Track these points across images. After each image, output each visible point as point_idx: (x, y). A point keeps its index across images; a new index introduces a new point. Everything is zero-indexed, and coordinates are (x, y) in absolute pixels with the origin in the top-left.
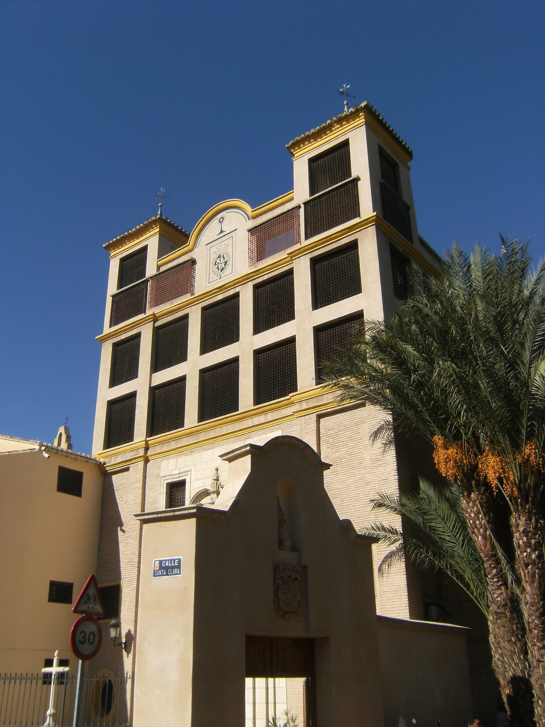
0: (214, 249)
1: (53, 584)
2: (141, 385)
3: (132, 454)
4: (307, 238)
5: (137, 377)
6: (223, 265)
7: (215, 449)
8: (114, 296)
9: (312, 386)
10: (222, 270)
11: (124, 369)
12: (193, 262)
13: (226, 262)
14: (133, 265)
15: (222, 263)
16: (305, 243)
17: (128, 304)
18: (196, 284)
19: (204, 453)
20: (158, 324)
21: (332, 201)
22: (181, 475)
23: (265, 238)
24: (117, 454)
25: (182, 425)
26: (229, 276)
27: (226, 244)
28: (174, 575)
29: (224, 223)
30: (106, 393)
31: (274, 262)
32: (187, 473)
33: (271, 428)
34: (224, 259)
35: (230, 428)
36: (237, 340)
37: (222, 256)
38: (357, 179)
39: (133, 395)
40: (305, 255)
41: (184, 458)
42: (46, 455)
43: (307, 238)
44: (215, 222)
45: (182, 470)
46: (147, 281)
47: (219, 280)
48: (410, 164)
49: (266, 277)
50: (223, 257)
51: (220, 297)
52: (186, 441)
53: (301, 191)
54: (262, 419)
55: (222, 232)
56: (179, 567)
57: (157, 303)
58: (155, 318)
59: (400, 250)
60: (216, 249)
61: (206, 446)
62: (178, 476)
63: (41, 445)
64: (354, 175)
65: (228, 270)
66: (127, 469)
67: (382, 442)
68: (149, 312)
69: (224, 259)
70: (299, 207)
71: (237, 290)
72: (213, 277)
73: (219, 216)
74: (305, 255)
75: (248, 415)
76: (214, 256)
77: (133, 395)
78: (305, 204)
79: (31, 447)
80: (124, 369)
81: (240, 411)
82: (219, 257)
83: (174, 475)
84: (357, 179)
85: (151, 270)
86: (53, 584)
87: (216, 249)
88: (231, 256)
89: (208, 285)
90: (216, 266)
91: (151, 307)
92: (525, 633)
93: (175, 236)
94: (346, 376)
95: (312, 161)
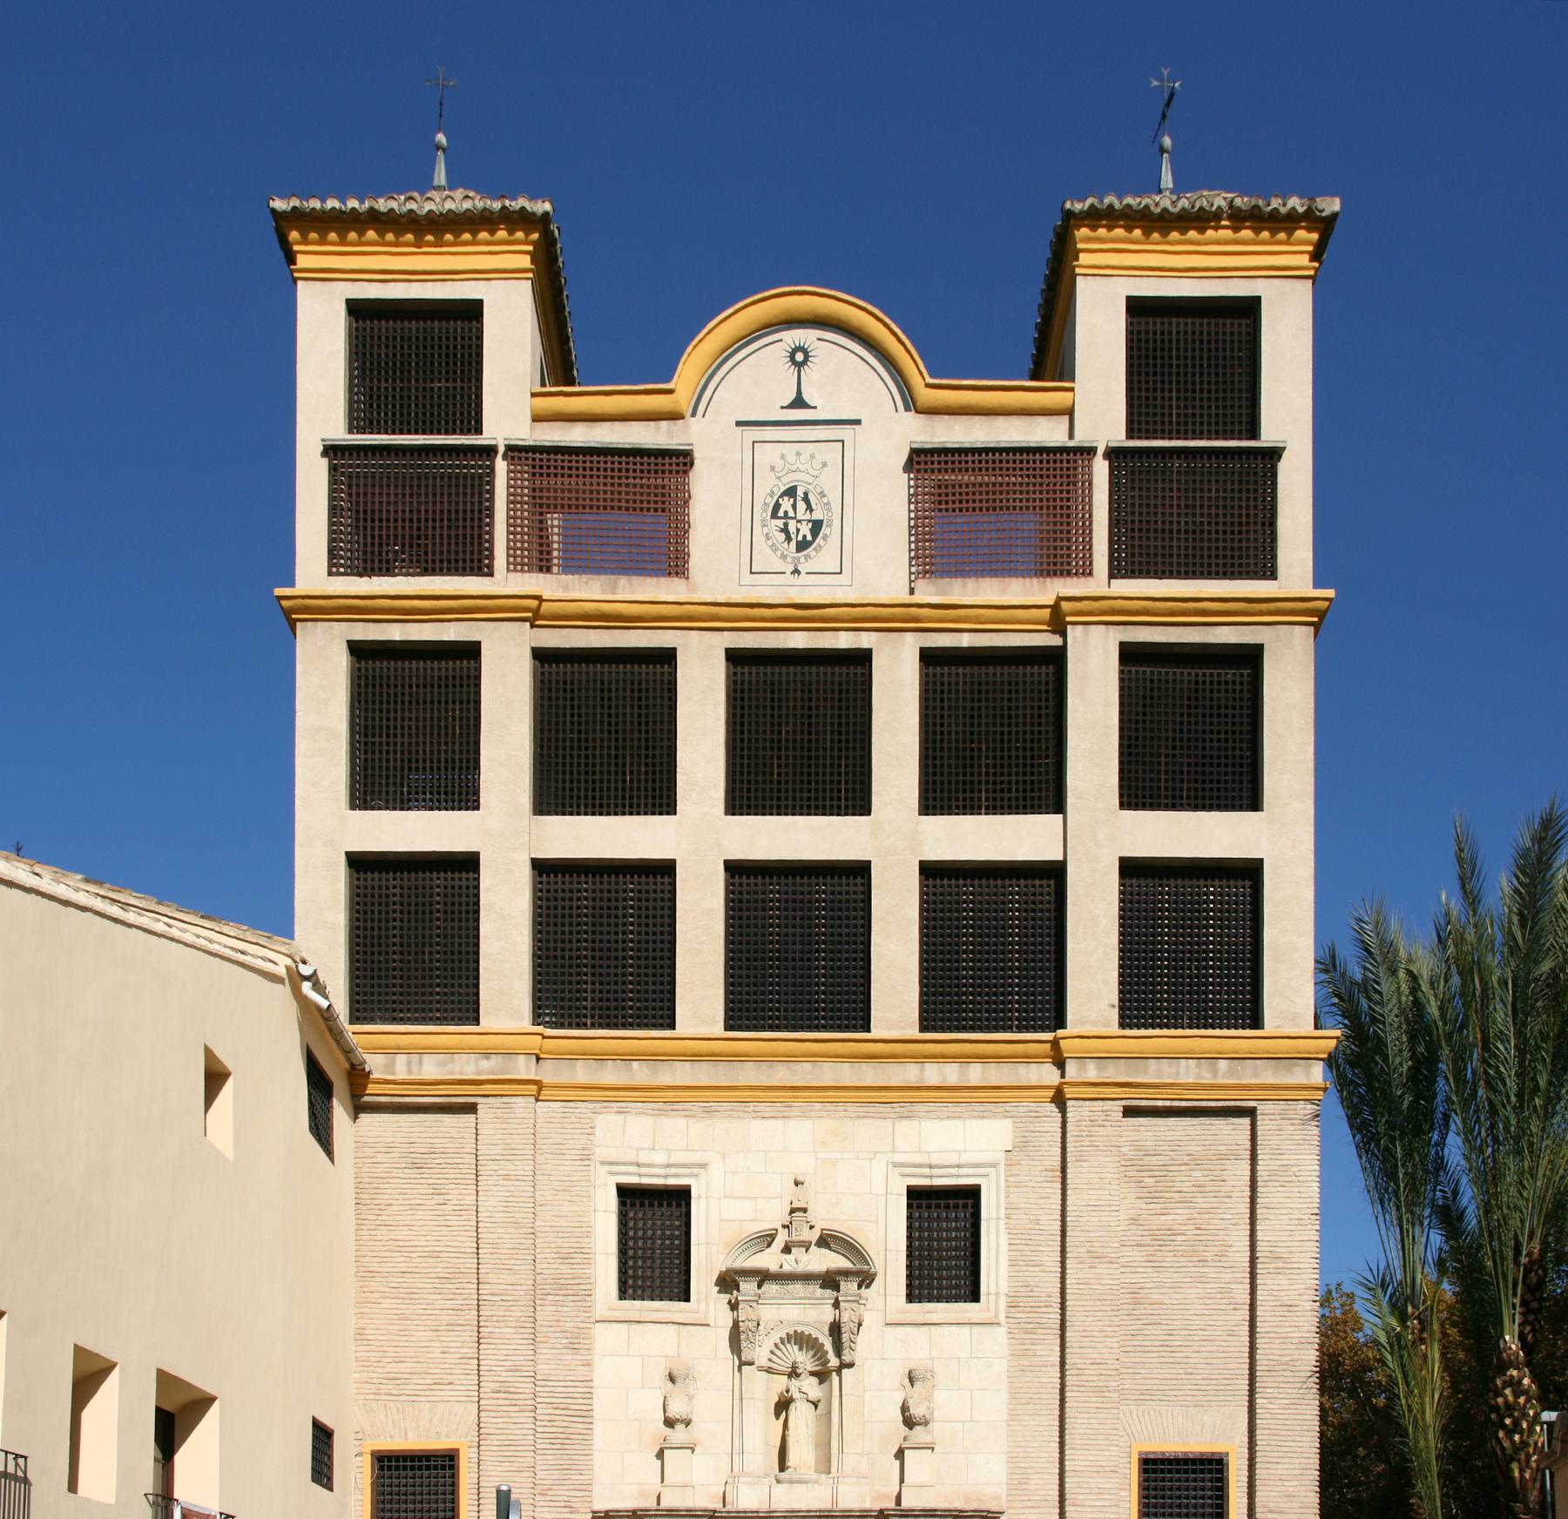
3: (485, 1064)
6: (805, 530)
7: (792, 1124)
9: (1108, 1025)
10: (803, 546)
13: (817, 526)
14: (414, 357)
19: (757, 1124)
24: (422, 1051)
27: (820, 458)
31: (1001, 604)
32: (695, 1171)
33: (977, 1107)
34: (809, 508)
35: (831, 1073)
37: (800, 492)
38: (1274, 454)
45: (678, 1157)
47: (789, 578)
49: (966, 641)
50: (806, 499)
51: (798, 640)
52: (681, 1074)
54: (933, 1074)
55: (799, 402)
61: (761, 1107)
66: (471, 1109)
69: (809, 508)
71: (864, 640)
81: (876, 1033)
82: (791, 492)
83: (938, 1167)
84: (1274, 454)
89: (748, 579)
90: (780, 523)
94: (324, 212)
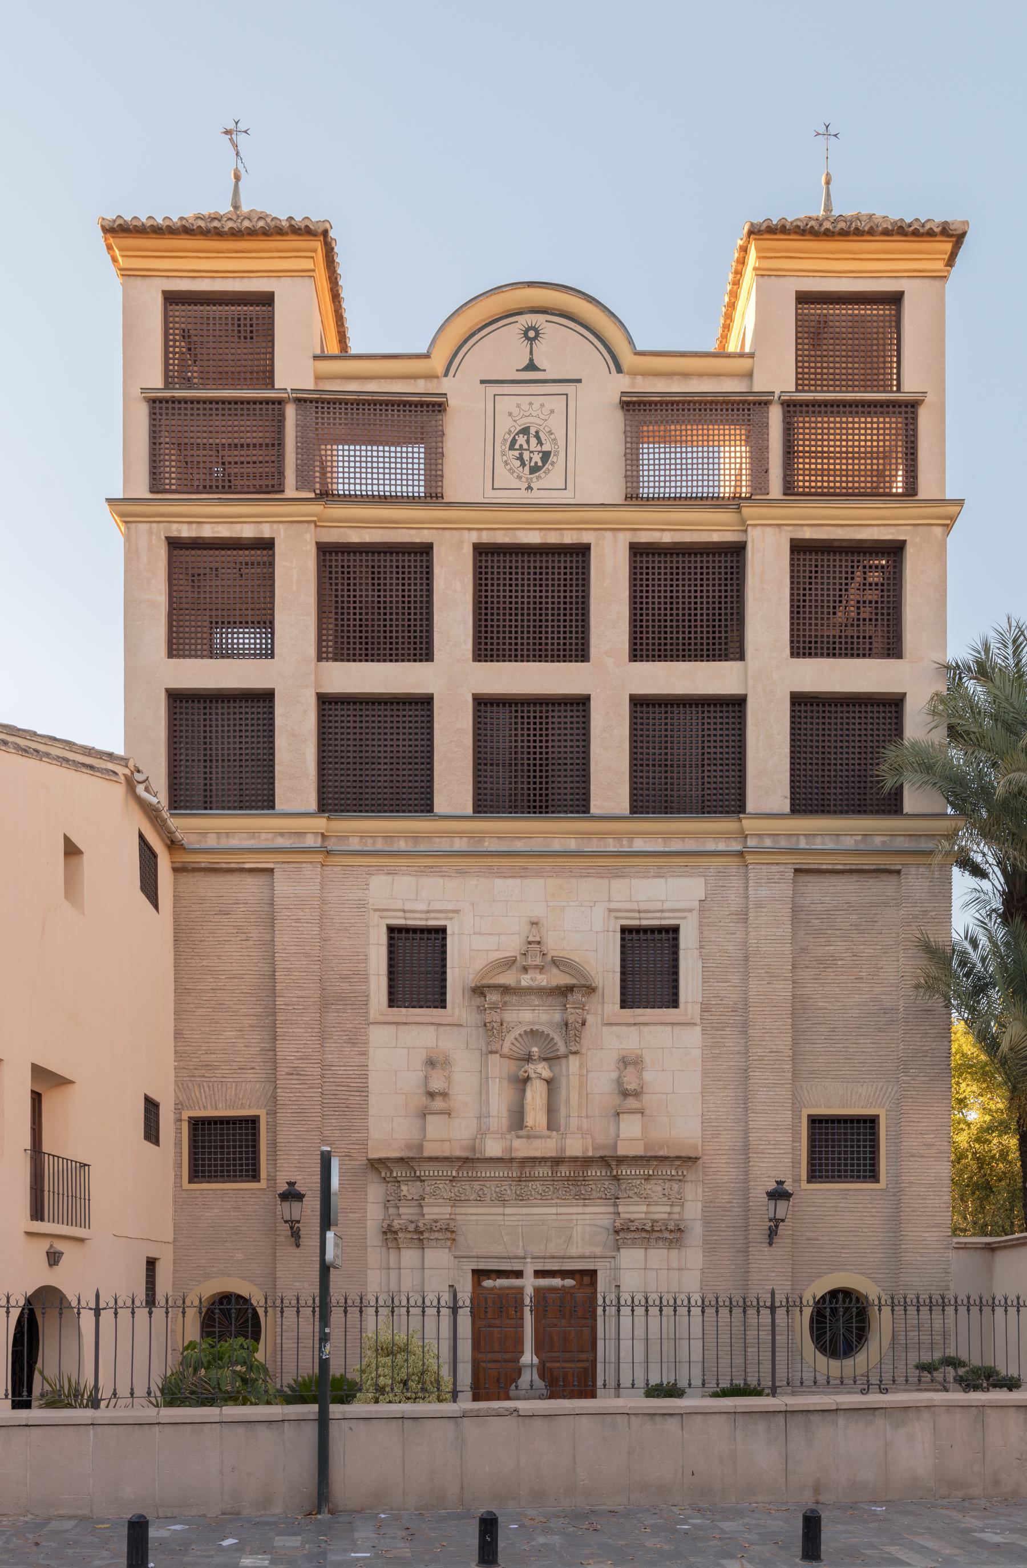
6: (537, 458)
7: (528, 882)
22: (432, 915)
32: (450, 915)
34: (540, 442)
37: (532, 431)
40: (541, 529)
41: (441, 880)
55: (531, 366)
62: (423, 916)
67: (977, 915)
69: (540, 442)
71: (585, 538)
74: (541, 529)
76: (506, 426)
81: (262, 1113)
82: (525, 431)
88: (562, 443)
90: (517, 453)
92: (1015, 641)
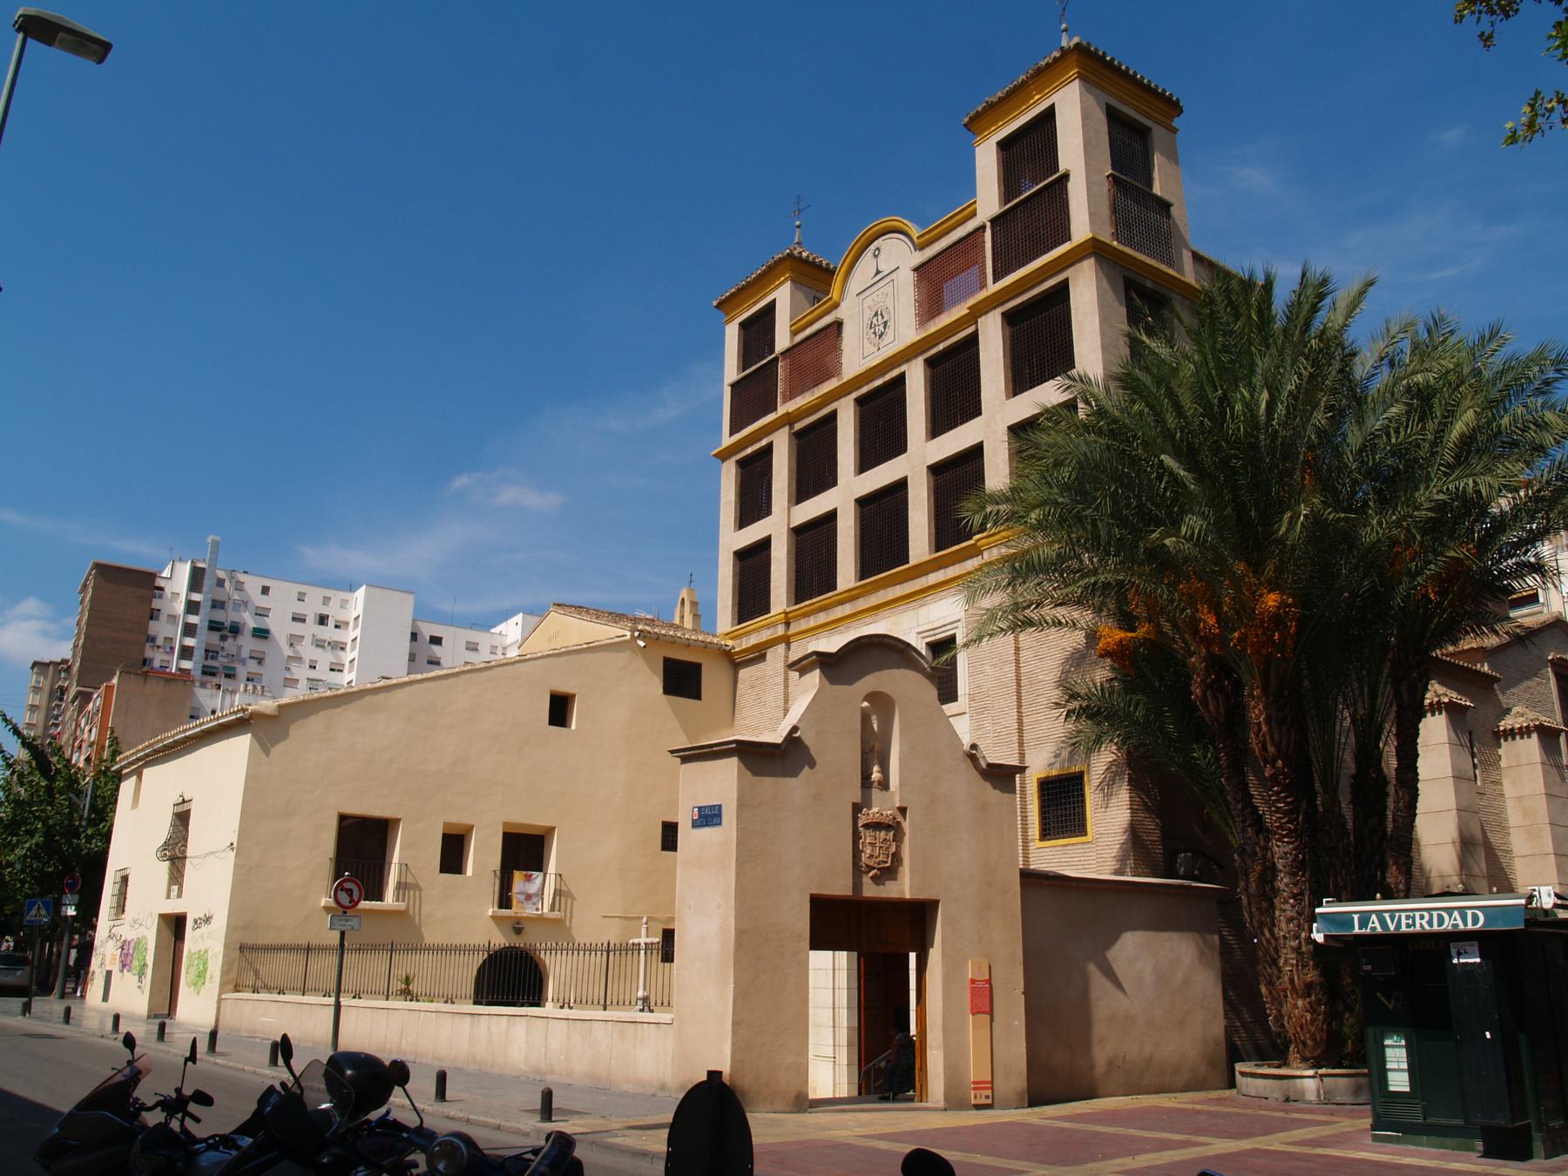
0: (868, 302)
1: (664, 849)
2: (777, 526)
4: (995, 280)
5: (835, 484)
8: (733, 386)
11: (753, 505)
12: (838, 325)
15: (879, 325)
16: (992, 288)
17: (753, 396)
18: (845, 360)
20: (798, 426)
21: (1033, 216)
23: (935, 281)
25: (768, 610)
26: (891, 347)
28: (856, 836)
29: (881, 257)
30: (734, 539)
36: (978, 413)
38: (1066, 177)
39: (831, 517)
42: (642, 644)
43: (995, 280)
44: (868, 255)
46: (776, 359)
48: (1176, 123)
53: (988, 201)
55: (878, 272)
56: (719, 815)
57: (791, 395)
58: (789, 420)
59: (1149, 284)
60: (872, 301)
63: (632, 631)
64: (1062, 167)
65: (888, 338)
68: (782, 409)
70: (982, 228)
72: (870, 349)
73: (873, 247)
75: (851, 595)
76: (869, 314)
77: (831, 517)
78: (994, 221)
79: (621, 632)
80: (753, 505)
85: (782, 341)
86: (664, 849)
87: (872, 301)
91: (784, 402)
93: (816, 278)
95: (1003, 145)
